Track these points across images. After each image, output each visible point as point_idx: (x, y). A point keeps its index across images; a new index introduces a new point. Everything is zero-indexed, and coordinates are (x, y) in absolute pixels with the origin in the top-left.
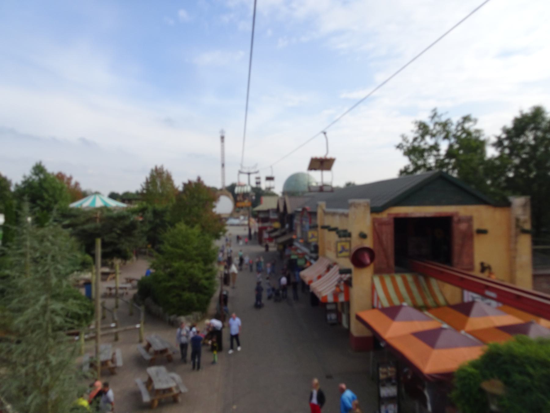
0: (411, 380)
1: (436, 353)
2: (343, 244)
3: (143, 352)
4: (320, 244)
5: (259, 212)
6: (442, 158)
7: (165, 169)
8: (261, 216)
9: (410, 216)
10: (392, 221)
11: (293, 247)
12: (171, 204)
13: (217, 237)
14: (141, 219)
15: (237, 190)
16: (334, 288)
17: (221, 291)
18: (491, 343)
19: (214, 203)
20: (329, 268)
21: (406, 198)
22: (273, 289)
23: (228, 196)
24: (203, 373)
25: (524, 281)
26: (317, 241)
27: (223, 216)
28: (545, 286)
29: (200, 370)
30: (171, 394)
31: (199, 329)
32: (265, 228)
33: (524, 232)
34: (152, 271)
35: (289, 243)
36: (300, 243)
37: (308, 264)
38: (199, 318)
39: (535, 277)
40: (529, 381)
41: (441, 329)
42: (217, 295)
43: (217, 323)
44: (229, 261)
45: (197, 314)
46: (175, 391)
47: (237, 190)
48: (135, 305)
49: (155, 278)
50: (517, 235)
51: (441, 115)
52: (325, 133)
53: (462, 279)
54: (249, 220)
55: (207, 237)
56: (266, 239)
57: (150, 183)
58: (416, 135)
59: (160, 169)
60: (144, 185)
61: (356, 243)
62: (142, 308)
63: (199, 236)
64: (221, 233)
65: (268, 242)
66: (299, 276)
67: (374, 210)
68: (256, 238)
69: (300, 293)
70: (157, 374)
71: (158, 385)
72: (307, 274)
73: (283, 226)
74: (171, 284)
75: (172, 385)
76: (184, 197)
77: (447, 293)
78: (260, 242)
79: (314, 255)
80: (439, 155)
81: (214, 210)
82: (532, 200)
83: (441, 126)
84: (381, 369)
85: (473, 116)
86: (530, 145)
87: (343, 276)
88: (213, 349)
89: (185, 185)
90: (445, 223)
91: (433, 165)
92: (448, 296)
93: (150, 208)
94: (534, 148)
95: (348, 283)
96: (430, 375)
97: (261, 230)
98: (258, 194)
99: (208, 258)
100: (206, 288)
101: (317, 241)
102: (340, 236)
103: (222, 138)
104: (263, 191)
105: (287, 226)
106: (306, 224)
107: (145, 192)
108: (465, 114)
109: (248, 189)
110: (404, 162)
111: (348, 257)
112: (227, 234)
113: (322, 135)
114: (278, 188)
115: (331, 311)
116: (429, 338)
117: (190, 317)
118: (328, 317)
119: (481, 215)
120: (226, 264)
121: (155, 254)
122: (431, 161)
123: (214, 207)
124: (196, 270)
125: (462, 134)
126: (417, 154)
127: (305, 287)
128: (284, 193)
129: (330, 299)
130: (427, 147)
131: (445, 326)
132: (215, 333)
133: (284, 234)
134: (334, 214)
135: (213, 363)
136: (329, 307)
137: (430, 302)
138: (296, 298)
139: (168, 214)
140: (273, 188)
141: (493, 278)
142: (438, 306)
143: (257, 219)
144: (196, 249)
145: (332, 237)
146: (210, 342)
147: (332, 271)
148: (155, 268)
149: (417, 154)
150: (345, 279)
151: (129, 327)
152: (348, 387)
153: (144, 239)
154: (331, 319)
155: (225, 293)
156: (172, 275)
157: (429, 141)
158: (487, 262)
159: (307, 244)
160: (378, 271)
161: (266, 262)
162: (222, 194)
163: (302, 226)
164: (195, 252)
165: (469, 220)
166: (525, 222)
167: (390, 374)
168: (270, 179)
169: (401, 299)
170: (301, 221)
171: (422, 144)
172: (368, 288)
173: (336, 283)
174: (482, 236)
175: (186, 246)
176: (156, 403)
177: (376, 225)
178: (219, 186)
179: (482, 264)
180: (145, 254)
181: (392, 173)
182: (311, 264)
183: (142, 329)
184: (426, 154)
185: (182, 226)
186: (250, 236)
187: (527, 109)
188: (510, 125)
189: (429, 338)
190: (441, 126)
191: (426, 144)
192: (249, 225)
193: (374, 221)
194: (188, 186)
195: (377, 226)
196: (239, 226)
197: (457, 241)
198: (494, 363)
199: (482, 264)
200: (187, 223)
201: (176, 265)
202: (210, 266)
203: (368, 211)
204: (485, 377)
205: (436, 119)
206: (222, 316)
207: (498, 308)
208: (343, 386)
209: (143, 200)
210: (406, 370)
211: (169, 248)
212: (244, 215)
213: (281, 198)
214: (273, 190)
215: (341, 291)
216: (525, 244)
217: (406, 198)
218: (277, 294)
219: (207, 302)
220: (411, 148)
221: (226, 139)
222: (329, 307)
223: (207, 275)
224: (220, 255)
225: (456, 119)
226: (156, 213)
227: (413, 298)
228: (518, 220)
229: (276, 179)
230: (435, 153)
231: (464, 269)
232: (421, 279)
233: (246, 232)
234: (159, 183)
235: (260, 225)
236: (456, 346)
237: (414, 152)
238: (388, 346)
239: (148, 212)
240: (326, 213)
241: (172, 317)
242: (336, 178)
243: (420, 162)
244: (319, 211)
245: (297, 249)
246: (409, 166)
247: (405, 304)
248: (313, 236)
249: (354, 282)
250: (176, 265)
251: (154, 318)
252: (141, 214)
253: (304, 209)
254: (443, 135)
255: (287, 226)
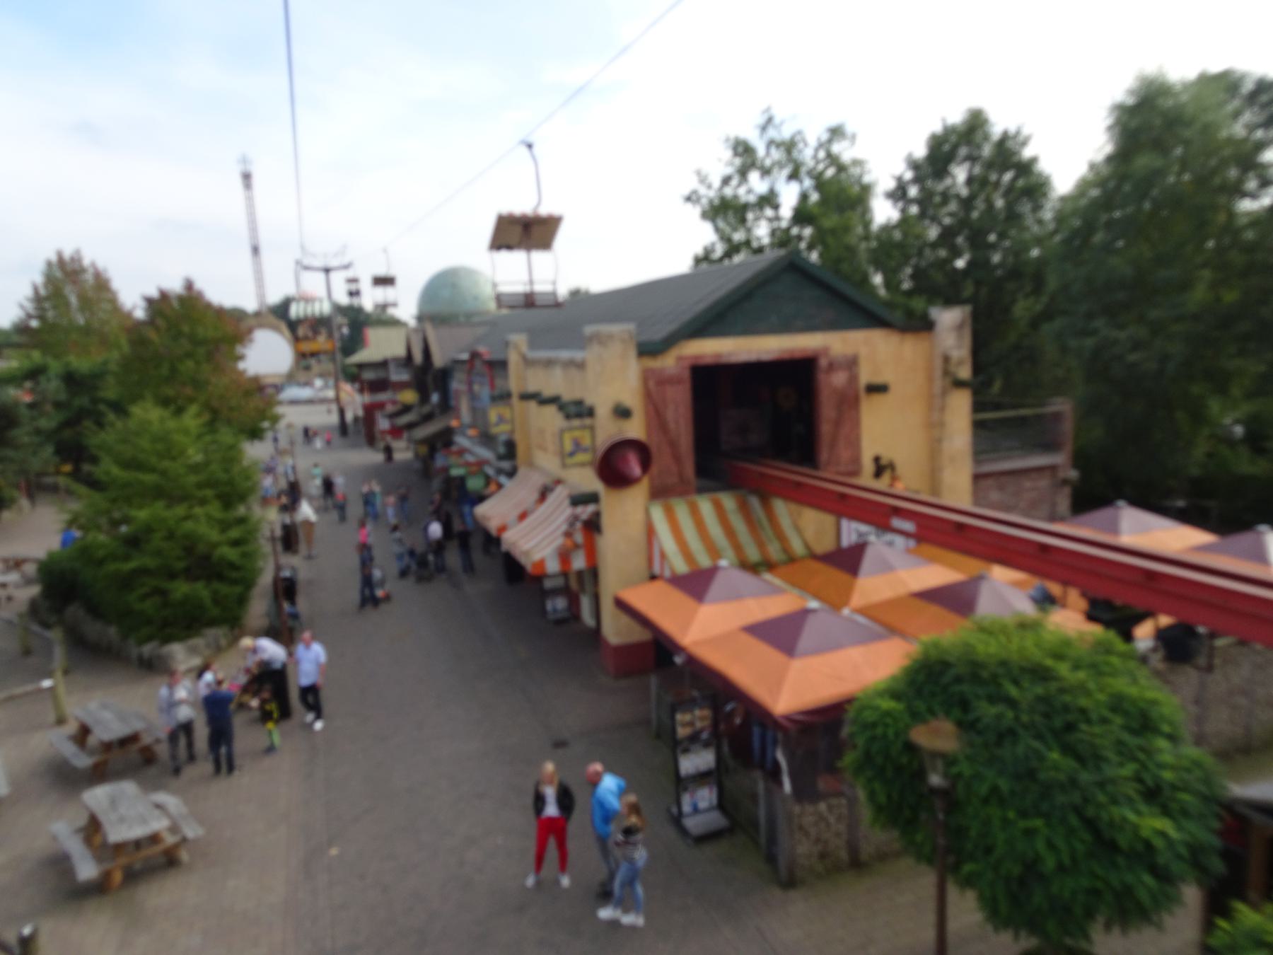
0: (741, 728)
1: (797, 666)
2: (577, 434)
3: (69, 750)
4: (518, 438)
5: (361, 366)
6: (784, 224)
7: (86, 262)
8: (369, 375)
9: (725, 360)
10: (686, 375)
11: (454, 448)
12: (115, 355)
13: (255, 434)
14: (27, 399)
15: (295, 311)
16: (560, 541)
17: (278, 568)
18: (925, 638)
19: (239, 349)
20: (544, 494)
21: (714, 321)
22: (412, 553)
23: (275, 328)
24: (245, 780)
25: (957, 490)
26: (512, 432)
27: (269, 381)
28: (995, 496)
29: (236, 773)
30: (157, 849)
31: (221, 676)
32: (381, 406)
33: (959, 384)
34: (77, 534)
35: (444, 440)
36: (470, 438)
37: (493, 487)
38: (223, 642)
39: (977, 478)
40: (1010, 714)
41: (805, 613)
42: (266, 579)
43: (271, 650)
44: (294, 493)
45: (218, 633)
46: (170, 840)
47: (295, 311)
48: (35, 628)
49: (85, 553)
50: (944, 393)
51: (782, 123)
52: (530, 146)
53: (844, 496)
54: (337, 388)
55: (226, 435)
56: (383, 432)
57: (47, 298)
58: (729, 170)
59: (72, 259)
60: (30, 306)
61: (607, 431)
62: (56, 635)
63: (199, 437)
64: (266, 424)
65: (389, 438)
66: (472, 514)
67: (646, 350)
68: (361, 430)
69: (478, 556)
70: (114, 802)
71: (117, 833)
72: (491, 512)
73: (424, 398)
74: (132, 565)
75: (158, 824)
76: (152, 335)
77: (808, 527)
78: (371, 440)
79: (506, 465)
80: (778, 218)
81: (241, 365)
82: (976, 317)
83: (782, 148)
84: (679, 717)
85: (849, 129)
86: (958, 196)
87: (579, 509)
88: (265, 716)
89: (150, 302)
90: (799, 374)
91: (766, 241)
92: (810, 534)
93: (55, 366)
94: (967, 203)
95: (593, 526)
96: (788, 718)
97: (370, 410)
98: (356, 323)
99: (232, 491)
100: (233, 566)
101: (512, 432)
102: (568, 417)
103: (247, 177)
104: (368, 316)
105: (435, 398)
106: (484, 391)
107: (34, 323)
108: (833, 122)
109: (325, 308)
110: (704, 235)
111: (591, 464)
112: (282, 425)
113: (524, 150)
114: (406, 309)
115: (555, 592)
116: (781, 634)
117: (198, 641)
118: (549, 605)
119: (874, 352)
120: (284, 500)
121: (82, 489)
122: (762, 232)
123: (241, 358)
124: (202, 524)
125: (826, 168)
126: (731, 214)
127: (492, 541)
128: (420, 318)
129: (553, 566)
130: (752, 199)
131: (813, 604)
132: (270, 681)
133: (428, 418)
134: (549, 363)
135: (270, 749)
136: (548, 584)
137: (774, 552)
138: (469, 567)
139: (111, 380)
140: (395, 305)
141: (899, 488)
142: (792, 559)
143: (357, 385)
144: (195, 468)
145: (550, 418)
146: (255, 703)
147: (552, 499)
148: (81, 527)
149: (731, 214)
150: (585, 517)
151: (19, 690)
152: (610, 769)
153: (48, 450)
154: (555, 611)
155: (286, 573)
156: (134, 542)
157: (757, 184)
158: (886, 457)
159: (487, 439)
160: (659, 493)
161: (386, 492)
162: (261, 326)
163: (473, 397)
164: (192, 479)
165: (852, 363)
166: (960, 363)
167: (699, 725)
168: (384, 281)
169: (714, 552)
170: (470, 384)
171: (742, 191)
172: (637, 530)
173: (564, 527)
174: (877, 399)
175: (166, 464)
176: (118, 877)
177: (651, 384)
178: (249, 304)
179: (877, 459)
180: (54, 489)
181: (679, 263)
182: (500, 486)
183: (61, 690)
184: (750, 216)
185: (147, 413)
186: (343, 428)
187: (956, 117)
188: (920, 151)
189: (781, 634)
190: (782, 148)
191: (750, 191)
192: (337, 399)
193: (646, 375)
194: (159, 305)
195: (653, 387)
196: (312, 405)
197: (827, 410)
198: (931, 682)
199: (877, 459)
200: (165, 402)
201: (142, 514)
202: (241, 510)
203: (632, 353)
204: (916, 717)
205: (772, 133)
206: (284, 632)
207: (908, 551)
208: (598, 767)
209: (35, 346)
210: (729, 707)
211: (116, 471)
212: (321, 375)
213: (416, 330)
214: (392, 311)
215: (576, 546)
216: (960, 406)
217: (714, 321)
218: (422, 563)
219: (242, 600)
220: (717, 202)
221: (257, 181)
222: (548, 584)
223: (234, 533)
224: (268, 482)
225: (814, 134)
226: (71, 380)
227: (737, 547)
228: (946, 359)
229: (399, 282)
230: (769, 212)
231: (839, 473)
232: (754, 502)
233: (334, 419)
234: (73, 300)
235: (368, 398)
236: (837, 646)
237: (725, 211)
238: (692, 661)
239: (49, 380)
240: (528, 362)
241: (147, 649)
242: (556, 272)
243: (738, 236)
244: (513, 358)
245: (462, 452)
246: (713, 244)
247: (723, 563)
248: (501, 420)
249: (606, 521)
250: (142, 514)
251: (92, 654)
252: (28, 384)
253: (475, 355)
254: (786, 172)
255: (435, 398)
